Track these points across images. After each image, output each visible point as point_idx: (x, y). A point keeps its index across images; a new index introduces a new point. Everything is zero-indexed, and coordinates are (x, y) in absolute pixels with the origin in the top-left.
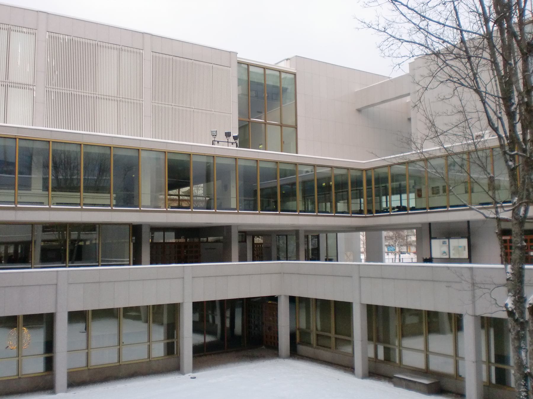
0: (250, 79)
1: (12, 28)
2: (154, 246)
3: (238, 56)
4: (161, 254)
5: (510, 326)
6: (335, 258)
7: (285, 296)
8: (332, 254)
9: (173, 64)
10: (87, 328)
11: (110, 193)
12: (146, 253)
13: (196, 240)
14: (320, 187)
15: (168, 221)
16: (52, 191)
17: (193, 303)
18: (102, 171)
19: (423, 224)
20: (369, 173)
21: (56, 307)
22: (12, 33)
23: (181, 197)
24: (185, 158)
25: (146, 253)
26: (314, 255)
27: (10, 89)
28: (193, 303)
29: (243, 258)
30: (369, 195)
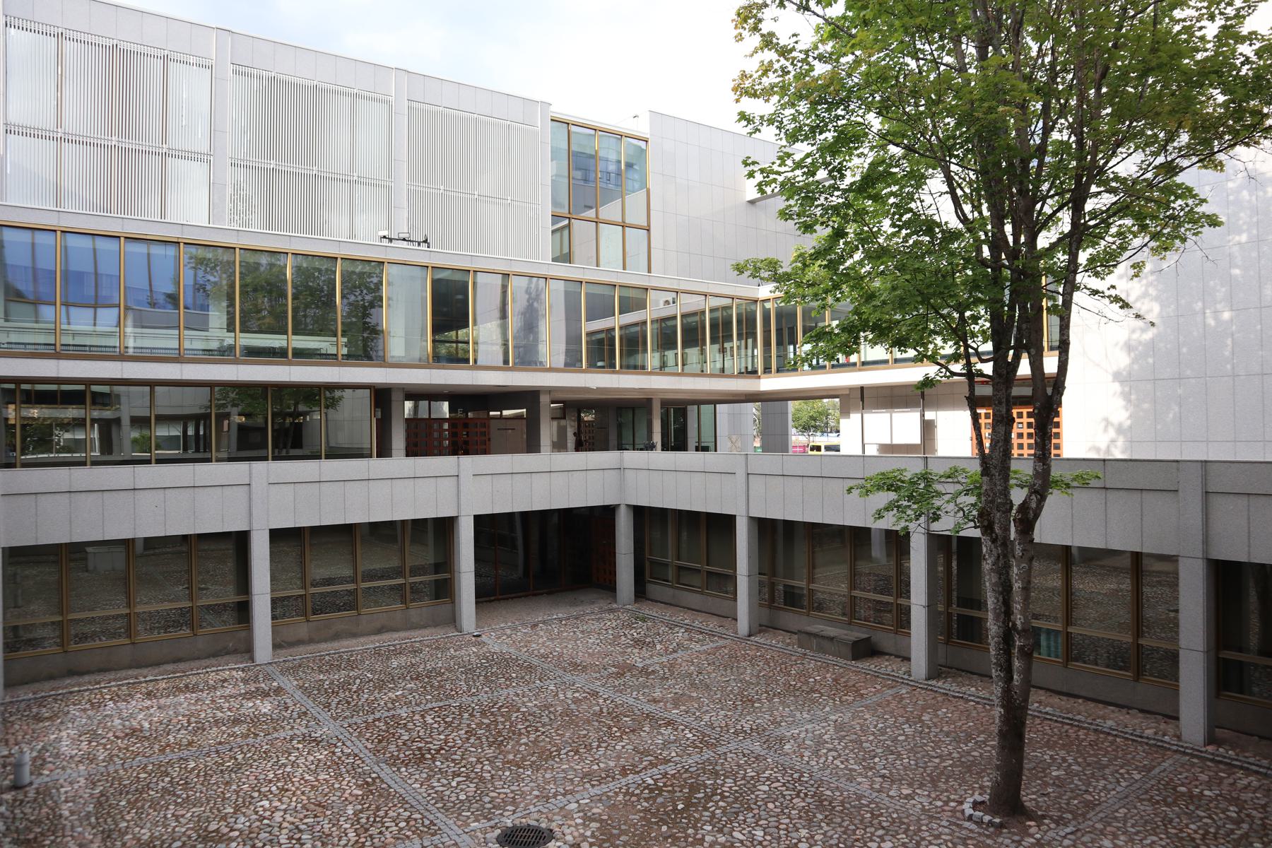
0: (574, 148)
1: (172, 56)
2: (413, 425)
3: (552, 108)
4: (423, 441)
5: (984, 550)
6: (712, 445)
7: (628, 506)
8: (707, 439)
9: (444, 128)
10: (303, 555)
11: (335, 335)
12: (398, 440)
13: (482, 415)
14: (714, 326)
15: (434, 382)
16: (588, 320)
17: (475, 516)
18: (331, 300)
19: (851, 389)
20: (768, 305)
21: (250, 523)
22: (171, 64)
23: (21, 632)
24: (458, 277)
25: (398, 440)
26: (676, 441)
27: (169, 160)
28: (475, 516)
29: (559, 446)
30: (767, 343)
